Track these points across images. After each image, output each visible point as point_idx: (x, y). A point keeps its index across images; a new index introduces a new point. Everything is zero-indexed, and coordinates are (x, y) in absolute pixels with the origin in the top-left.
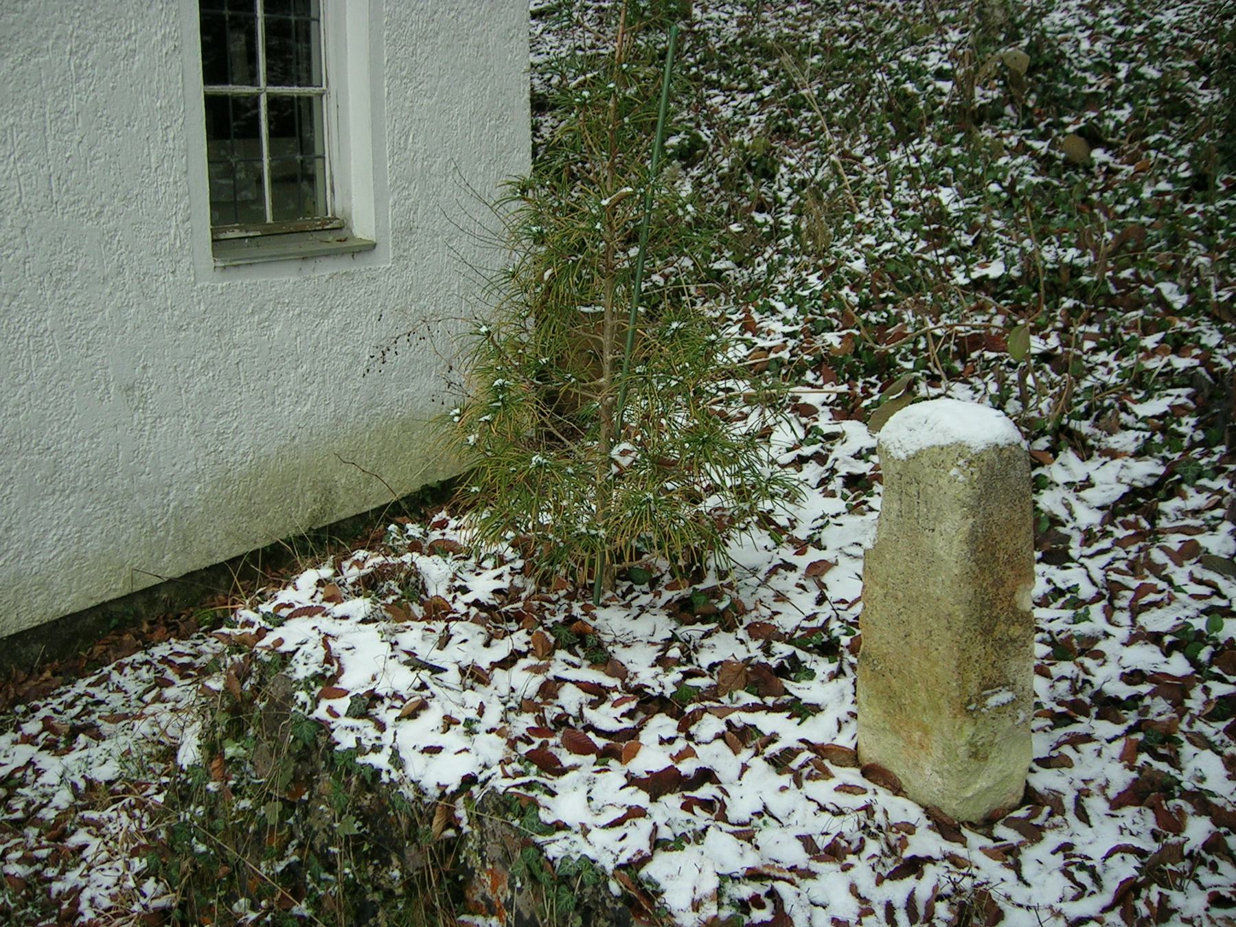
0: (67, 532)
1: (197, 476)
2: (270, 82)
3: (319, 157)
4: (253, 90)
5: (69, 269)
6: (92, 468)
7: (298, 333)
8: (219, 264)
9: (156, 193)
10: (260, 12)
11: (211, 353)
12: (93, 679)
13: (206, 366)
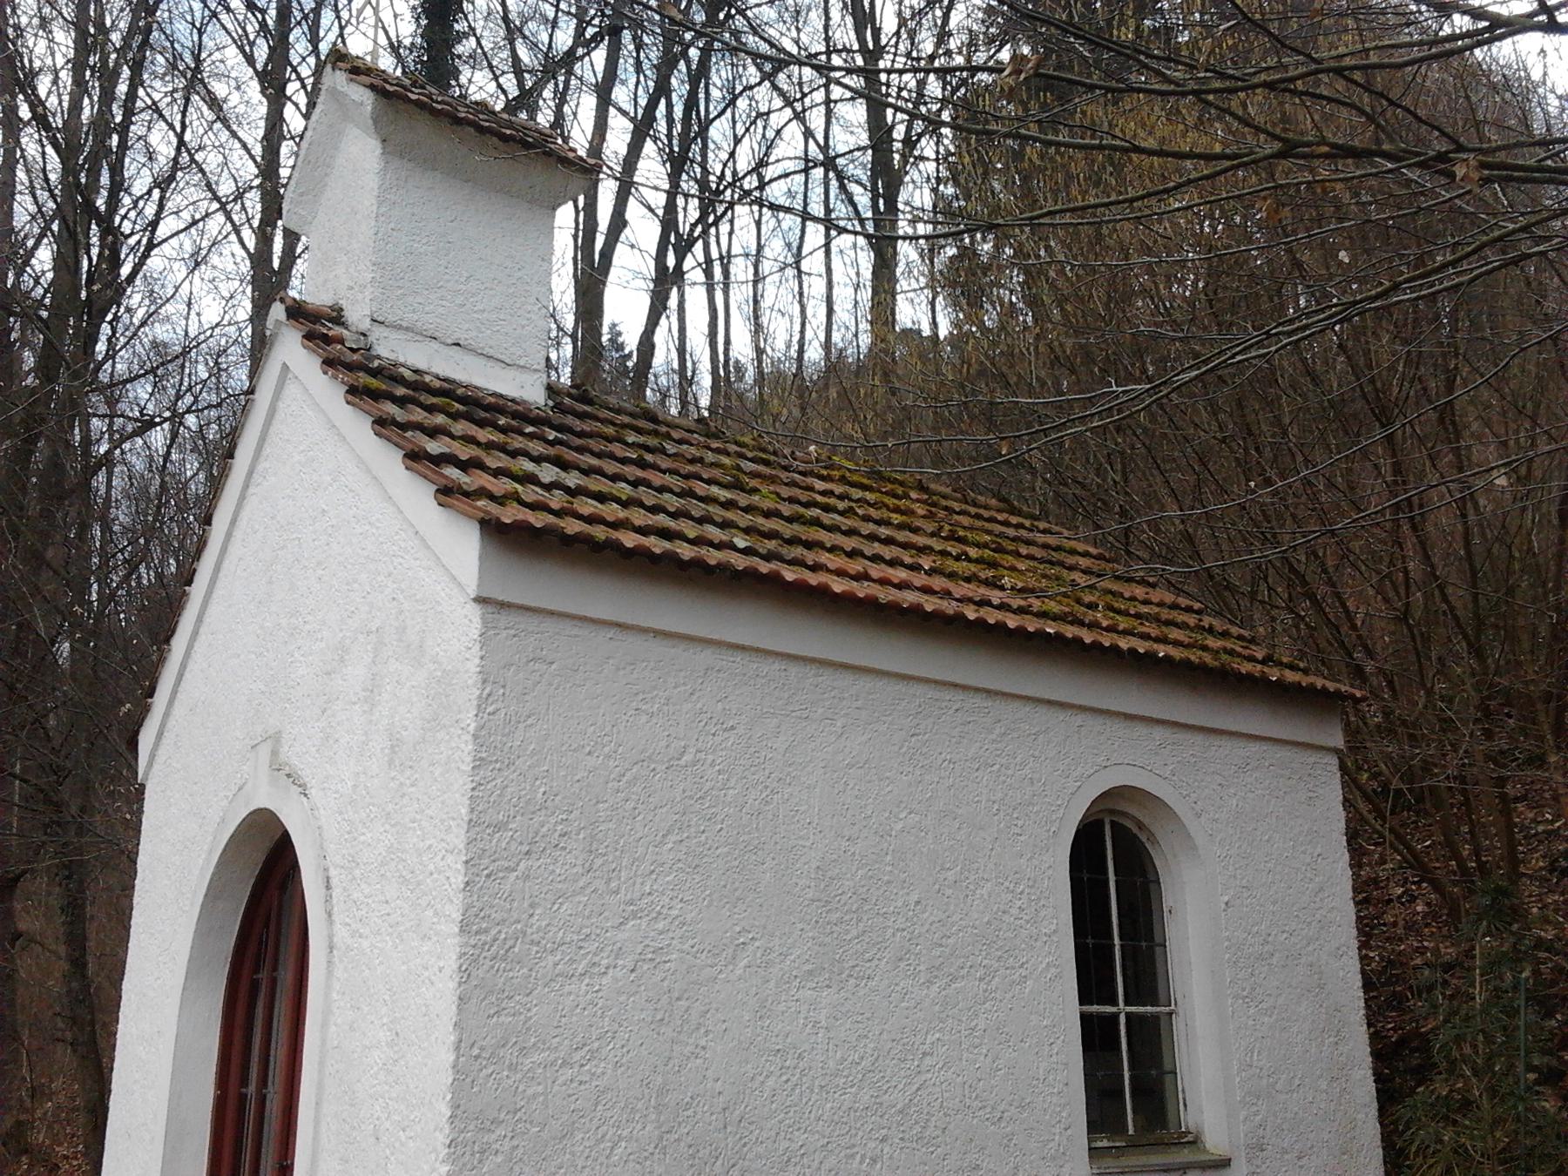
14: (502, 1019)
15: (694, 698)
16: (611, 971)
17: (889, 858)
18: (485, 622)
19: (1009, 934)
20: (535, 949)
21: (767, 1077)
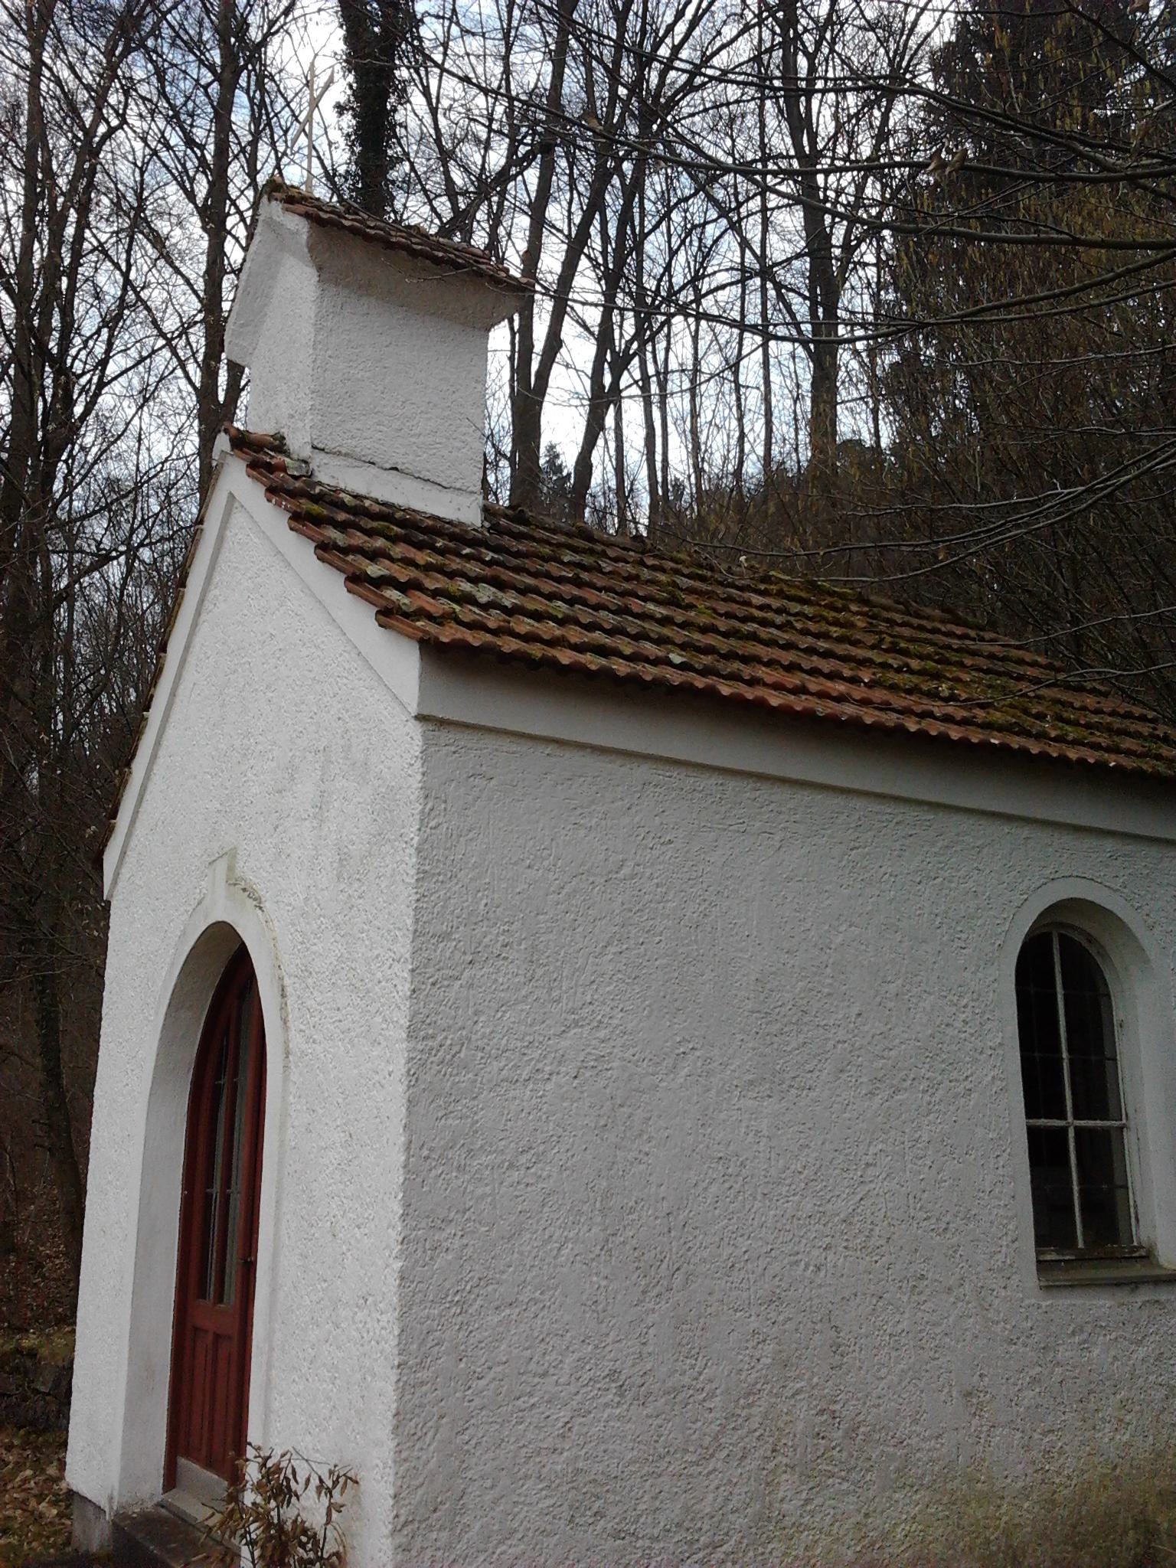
0: (913, 1529)
1: (1026, 1493)
2: (1076, 1117)
3: (1121, 1187)
4: (1071, 1134)
5: (922, 1277)
7: (1115, 1358)
9: (990, 1214)
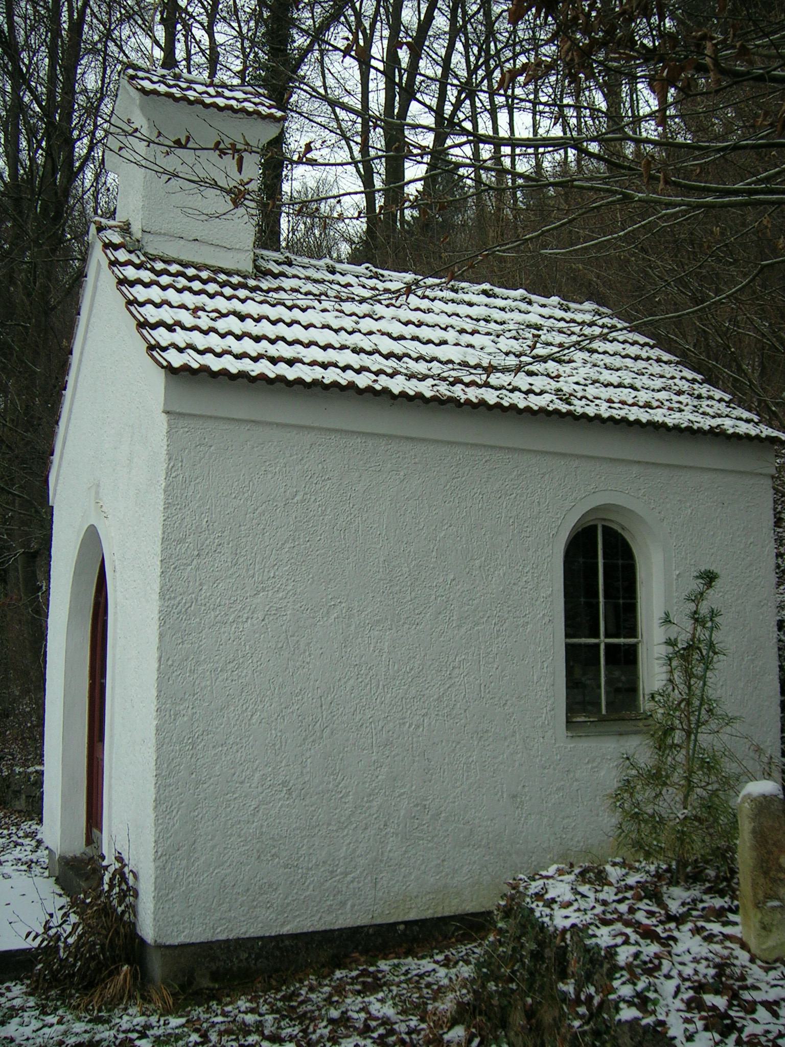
5: (487, 731)
6: (490, 836)
8: (569, 734)
10: (601, 599)
11: (562, 783)
12: (476, 944)
13: (558, 789)
14: (185, 645)
15: (303, 462)
16: (249, 621)
17: (434, 553)
18: (169, 425)
19: (517, 597)
20: (203, 608)
21: (349, 679)
